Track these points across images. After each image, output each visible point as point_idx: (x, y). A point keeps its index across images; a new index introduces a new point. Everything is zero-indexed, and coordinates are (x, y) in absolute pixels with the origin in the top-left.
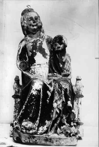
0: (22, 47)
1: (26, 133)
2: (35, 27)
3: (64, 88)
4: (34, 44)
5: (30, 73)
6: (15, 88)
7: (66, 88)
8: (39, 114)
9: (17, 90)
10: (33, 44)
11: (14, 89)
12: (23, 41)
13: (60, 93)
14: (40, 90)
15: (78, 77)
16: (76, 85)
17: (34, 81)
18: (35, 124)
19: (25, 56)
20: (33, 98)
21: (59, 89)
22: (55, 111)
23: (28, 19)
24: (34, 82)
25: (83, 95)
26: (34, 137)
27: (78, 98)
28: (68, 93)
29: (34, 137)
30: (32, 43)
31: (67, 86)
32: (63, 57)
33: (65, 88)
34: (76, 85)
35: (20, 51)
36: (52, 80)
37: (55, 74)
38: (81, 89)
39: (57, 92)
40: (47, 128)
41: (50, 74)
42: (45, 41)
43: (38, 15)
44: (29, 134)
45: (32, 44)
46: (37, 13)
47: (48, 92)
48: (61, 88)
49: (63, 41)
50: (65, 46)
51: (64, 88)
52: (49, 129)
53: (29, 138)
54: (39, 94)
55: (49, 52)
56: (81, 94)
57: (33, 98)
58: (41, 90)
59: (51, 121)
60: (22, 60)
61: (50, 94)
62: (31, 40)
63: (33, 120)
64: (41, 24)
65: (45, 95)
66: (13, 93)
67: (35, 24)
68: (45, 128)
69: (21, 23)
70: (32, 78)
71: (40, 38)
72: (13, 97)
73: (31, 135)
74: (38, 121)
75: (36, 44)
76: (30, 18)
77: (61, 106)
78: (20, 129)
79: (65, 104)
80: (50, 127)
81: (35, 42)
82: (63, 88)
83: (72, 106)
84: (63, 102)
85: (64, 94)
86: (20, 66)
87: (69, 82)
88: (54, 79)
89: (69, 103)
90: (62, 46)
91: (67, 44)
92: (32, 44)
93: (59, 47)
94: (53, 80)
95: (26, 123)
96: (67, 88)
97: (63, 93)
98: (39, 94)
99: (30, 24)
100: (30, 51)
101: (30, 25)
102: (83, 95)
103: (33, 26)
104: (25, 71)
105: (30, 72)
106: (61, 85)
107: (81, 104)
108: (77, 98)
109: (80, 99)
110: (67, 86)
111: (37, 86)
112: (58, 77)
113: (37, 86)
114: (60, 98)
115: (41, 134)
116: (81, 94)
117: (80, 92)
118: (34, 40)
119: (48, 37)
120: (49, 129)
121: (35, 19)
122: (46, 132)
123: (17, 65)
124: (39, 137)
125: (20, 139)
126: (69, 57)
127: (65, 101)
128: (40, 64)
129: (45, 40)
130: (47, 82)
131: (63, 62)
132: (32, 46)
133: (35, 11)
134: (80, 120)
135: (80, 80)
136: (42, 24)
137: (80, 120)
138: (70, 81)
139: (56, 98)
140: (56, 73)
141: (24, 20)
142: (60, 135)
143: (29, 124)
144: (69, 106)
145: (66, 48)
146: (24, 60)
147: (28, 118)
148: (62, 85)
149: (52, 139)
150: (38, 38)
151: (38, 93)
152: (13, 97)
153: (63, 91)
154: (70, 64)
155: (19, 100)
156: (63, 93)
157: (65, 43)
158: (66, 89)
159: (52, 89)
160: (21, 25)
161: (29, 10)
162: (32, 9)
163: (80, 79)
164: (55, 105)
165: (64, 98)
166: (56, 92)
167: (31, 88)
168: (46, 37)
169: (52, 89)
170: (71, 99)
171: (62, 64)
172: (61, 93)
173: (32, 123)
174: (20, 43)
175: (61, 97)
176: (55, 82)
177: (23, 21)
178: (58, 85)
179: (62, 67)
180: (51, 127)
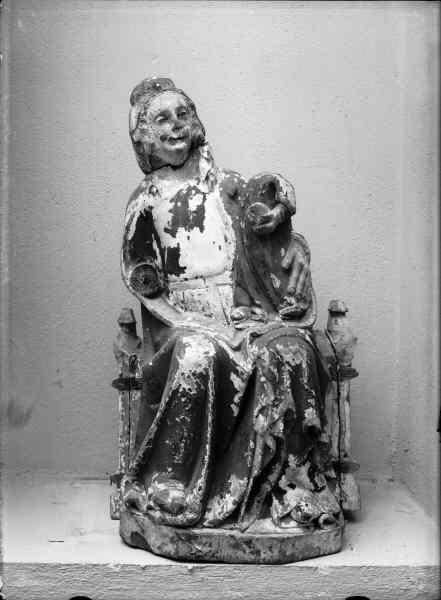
0: (137, 215)
1: (163, 522)
2: (181, 145)
3: (290, 365)
4: (179, 204)
5: (169, 306)
6: (118, 355)
7: (298, 362)
8: (206, 458)
9: (127, 362)
10: (176, 206)
11: (116, 357)
12: (141, 196)
13: (276, 384)
14: (208, 375)
15: (336, 306)
16: (330, 331)
17: (185, 340)
18: (192, 493)
19: (151, 245)
20: (183, 400)
21: (272, 368)
22: (260, 442)
23: (156, 117)
24: (184, 346)
25: (358, 371)
26: (191, 538)
27: (338, 381)
28: (306, 381)
29: (191, 538)
30: (171, 201)
31: (302, 355)
32: (283, 250)
33: (293, 364)
34: (330, 331)
35: (133, 228)
36: (246, 335)
37: (258, 311)
38: (348, 350)
39: (267, 378)
40: (235, 503)
41: (239, 312)
42: (217, 190)
43: (188, 99)
44: (177, 526)
45: (173, 204)
46: (182, 93)
47: (233, 377)
48: (279, 364)
49: (281, 194)
50: (289, 211)
51: (290, 365)
52: (243, 508)
53: (172, 541)
54: (202, 387)
55: (233, 232)
56: (350, 366)
57: (183, 400)
58: (211, 373)
59: (249, 479)
60: (139, 262)
61: (238, 383)
62: (170, 186)
63: (185, 475)
64: (200, 132)
65: (224, 389)
66: (116, 371)
67: (180, 133)
68: (228, 503)
69: (132, 133)
70: (178, 329)
71: (198, 179)
72: (116, 384)
73: (180, 531)
74: (201, 482)
75: (186, 204)
76: (160, 115)
77: (281, 426)
78: (144, 508)
79: (292, 419)
80: (246, 500)
81: (182, 198)
82: (288, 363)
83: (319, 426)
84: (287, 415)
85: (292, 386)
86: (134, 280)
87: (308, 338)
88: (251, 331)
89: (310, 415)
90: (276, 212)
91: (293, 205)
92: (173, 204)
93: (268, 219)
94: (252, 335)
95: (162, 487)
96: (301, 364)
97: (289, 382)
98: (202, 387)
99: (162, 134)
100: (166, 230)
101: (163, 138)
102: (354, 371)
103: (173, 141)
104: (151, 296)
105: (171, 303)
106: (278, 353)
107: (348, 399)
108: (334, 383)
109: (345, 385)
110: (302, 355)
111: (194, 355)
112: (266, 323)
113: (194, 355)
114: (276, 399)
115: (217, 524)
116: (350, 366)
117: (346, 358)
118: (179, 189)
119: (228, 176)
120: (243, 508)
121: (178, 115)
122: (233, 517)
123: (124, 279)
124: (209, 536)
125: (144, 539)
126: (304, 247)
127: (294, 410)
128: (202, 277)
129: (218, 186)
130: (226, 338)
131: (283, 268)
132: (170, 211)
133: (177, 86)
134: (346, 456)
135: (342, 314)
136: (203, 129)
137: (346, 456)
138: (310, 336)
139: (263, 399)
140: (259, 306)
141: (140, 120)
142: (283, 525)
143: (175, 493)
144: (310, 424)
145: (293, 218)
146: (148, 261)
147: (170, 470)
148: (283, 355)
149: (254, 541)
150: (193, 183)
151: (199, 386)
152: (116, 384)
153: (286, 376)
154: (308, 275)
155: (137, 395)
156: (288, 383)
157: (289, 202)
158: (297, 369)
159: (246, 366)
160: (133, 139)
161: (155, 84)
162: (168, 81)
163: (343, 309)
164: (261, 422)
165: (290, 397)
166: (263, 379)
167: (171, 368)
168: (222, 177)
169: (246, 366)
170: (317, 401)
171: (279, 278)
172: (281, 381)
173: (181, 486)
174: (131, 199)
175: (283, 397)
176: (257, 340)
177: (137, 127)
178: (268, 353)
179: (281, 285)
180: (249, 499)
